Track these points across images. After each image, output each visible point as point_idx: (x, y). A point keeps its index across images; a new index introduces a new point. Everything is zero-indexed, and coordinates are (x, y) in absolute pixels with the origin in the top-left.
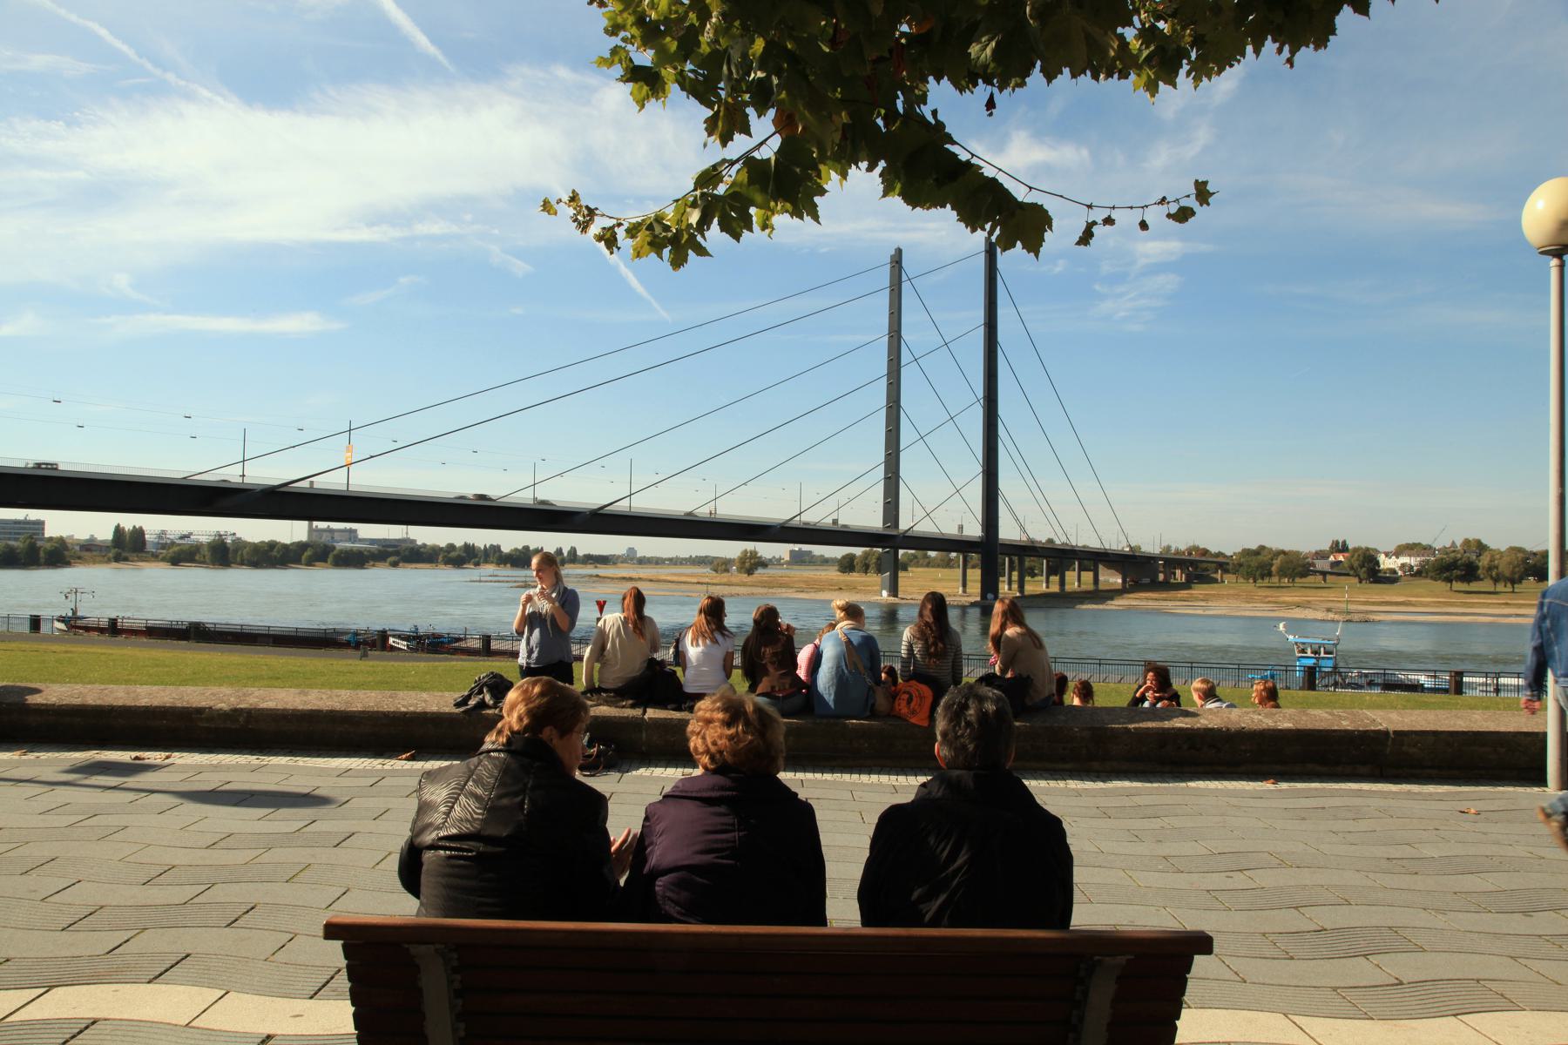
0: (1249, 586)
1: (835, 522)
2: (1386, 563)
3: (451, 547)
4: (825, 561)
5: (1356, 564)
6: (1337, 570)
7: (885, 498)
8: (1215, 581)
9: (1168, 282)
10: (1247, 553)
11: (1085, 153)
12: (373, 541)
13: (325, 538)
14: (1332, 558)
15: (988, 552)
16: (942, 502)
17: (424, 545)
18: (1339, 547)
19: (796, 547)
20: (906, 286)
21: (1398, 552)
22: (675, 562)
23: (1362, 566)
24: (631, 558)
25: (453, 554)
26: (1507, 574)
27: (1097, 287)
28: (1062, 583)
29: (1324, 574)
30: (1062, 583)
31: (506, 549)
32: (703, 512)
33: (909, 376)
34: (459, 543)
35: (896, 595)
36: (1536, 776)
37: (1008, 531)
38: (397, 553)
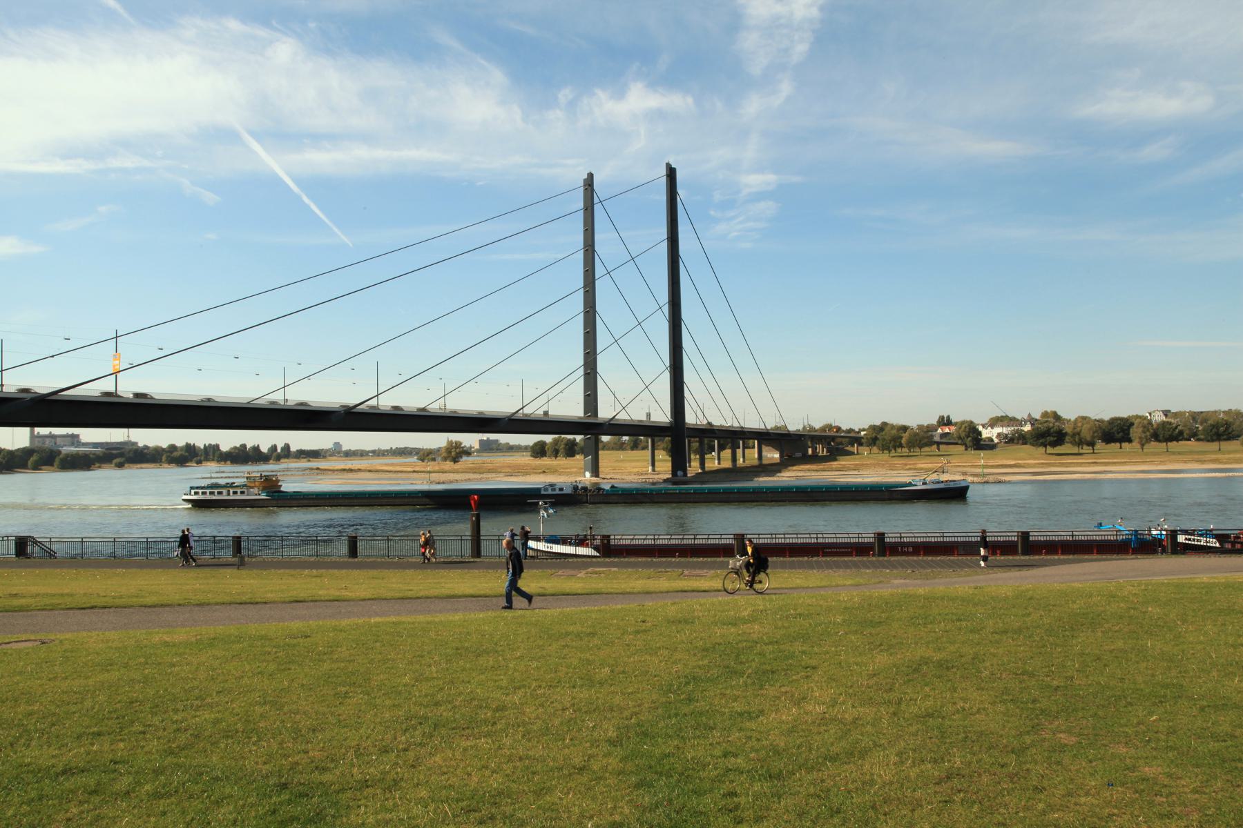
0: (885, 456)
1: (546, 413)
2: (986, 433)
3: (173, 448)
4: (511, 448)
5: (963, 435)
6: (947, 440)
7: (585, 391)
8: (852, 453)
9: (768, 208)
10: (873, 428)
11: (690, 100)
12: (96, 445)
13: (48, 444)
14: (940, 431)
15: (678, 436)
16: (634, 393)
17: (146, 447)
18: (945, 421)
19: (485, 436)
20: (597, 208)
21: (994, 422)
22: (378, 453)
23: (968, 436)
24: (337, 451)
25: (176, 454)
26: (1089, 439)
27: (712, 213)
28: (734, 459)
29: (938, 444)
30: (734, 459)
31: (225, 448)
32: (435, 407)
33: (603, 288)
34: (180, 443)
35: (597, 476)
36: (473, 556)
37: (605, 412)
38: (121, 455)
